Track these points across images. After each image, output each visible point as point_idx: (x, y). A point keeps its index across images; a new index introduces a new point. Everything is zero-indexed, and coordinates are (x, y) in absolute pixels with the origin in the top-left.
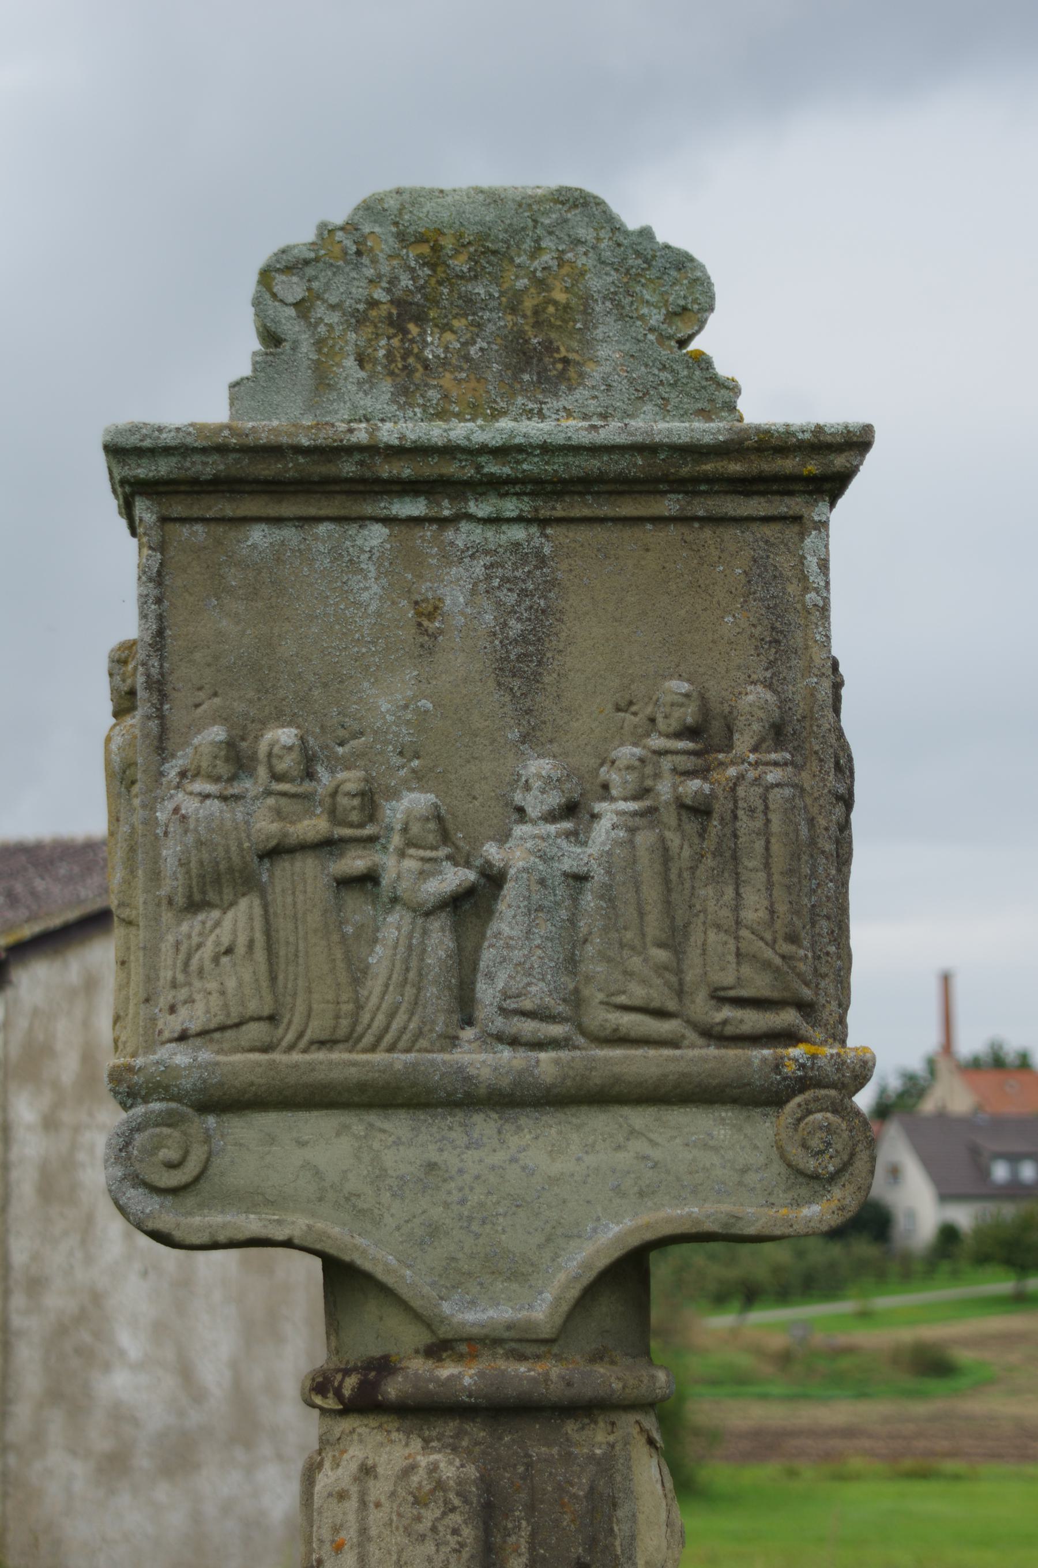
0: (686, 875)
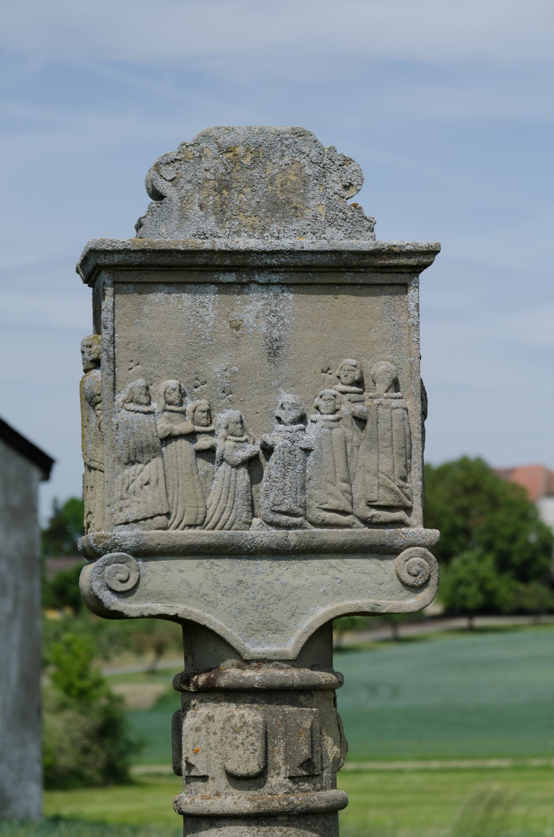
0: (355, 449)
